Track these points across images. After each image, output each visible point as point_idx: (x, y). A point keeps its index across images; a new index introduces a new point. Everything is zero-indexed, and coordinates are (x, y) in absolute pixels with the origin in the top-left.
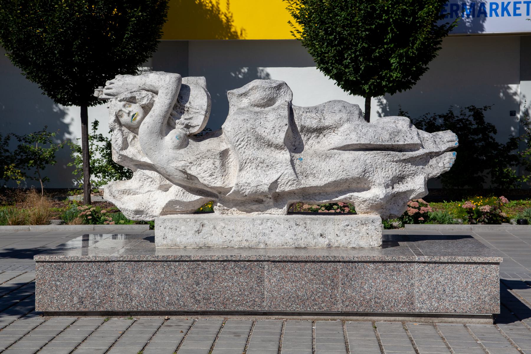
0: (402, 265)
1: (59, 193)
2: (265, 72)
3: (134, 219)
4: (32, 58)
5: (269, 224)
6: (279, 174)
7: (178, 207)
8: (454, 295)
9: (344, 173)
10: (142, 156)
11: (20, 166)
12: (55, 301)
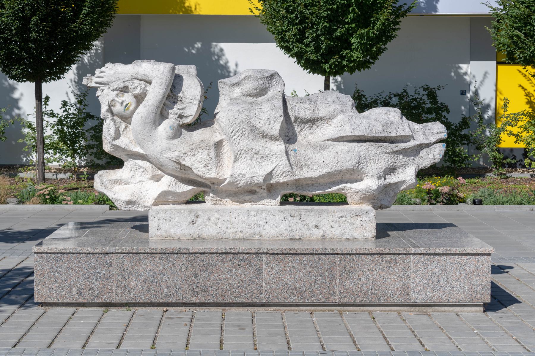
0: (398, 257)
2: (219, 48)
5: (264, 215)
6: (274, 165)
7: (170, 197)
8: (448, 285)
9: (339, 164)
10: (135, 146)
12: (54, 292)
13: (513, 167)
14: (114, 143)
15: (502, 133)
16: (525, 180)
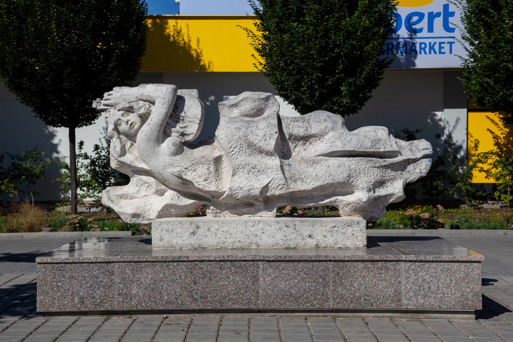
0: (389, 263)
1: (49, 204)
3: (132, 222)
4: (26, 84)
5: (261, 226)
6: (270, 179)
7: (173, 210)
8: (439, 292)
10: (140, 163)
11: (13, 181)
13: (484, 199)
14: (120, 159)
15: (474, 169)
16: (496, 211)
